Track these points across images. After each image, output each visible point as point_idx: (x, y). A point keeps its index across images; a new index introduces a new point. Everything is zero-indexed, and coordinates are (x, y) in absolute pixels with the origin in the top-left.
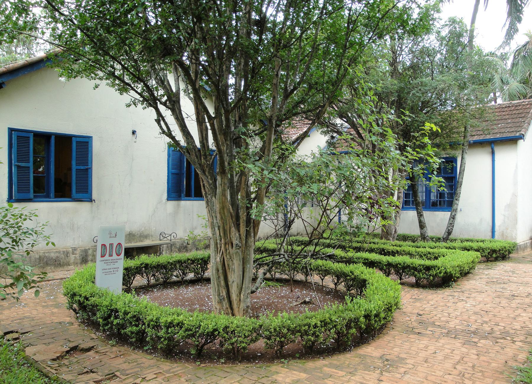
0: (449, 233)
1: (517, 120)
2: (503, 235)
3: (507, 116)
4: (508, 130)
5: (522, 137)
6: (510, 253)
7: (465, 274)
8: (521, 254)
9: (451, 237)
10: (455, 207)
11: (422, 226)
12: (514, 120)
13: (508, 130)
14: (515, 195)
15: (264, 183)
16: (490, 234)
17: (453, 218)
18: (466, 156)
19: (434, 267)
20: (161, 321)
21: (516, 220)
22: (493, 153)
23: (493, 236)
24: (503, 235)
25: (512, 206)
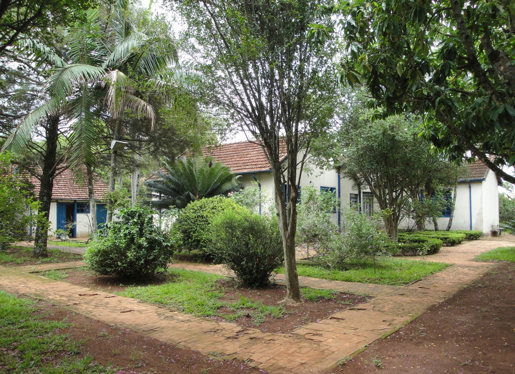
0: (449, 227)
1: (482, 170)
2: (476, 229)
3: (477, 167)
4: (477, 175)
5: (484, 179)
6: (479, 236)
7: (459, 242)
8: (485, 238)
9: (450, 230)
10: (452, 215)
11: (436, 224)
12: (480, 170)
13: (477, 175)
14: (481, 209)
15: (344, 15)
16: (469, 228)
17: (451, 220)
18: (457, 190)
19: (448, 238)
20: (135, 46)
21: (482, 221)
22: (470, 187)
23: (471, 229)
24: (476, 229)
25: (480, 214)
